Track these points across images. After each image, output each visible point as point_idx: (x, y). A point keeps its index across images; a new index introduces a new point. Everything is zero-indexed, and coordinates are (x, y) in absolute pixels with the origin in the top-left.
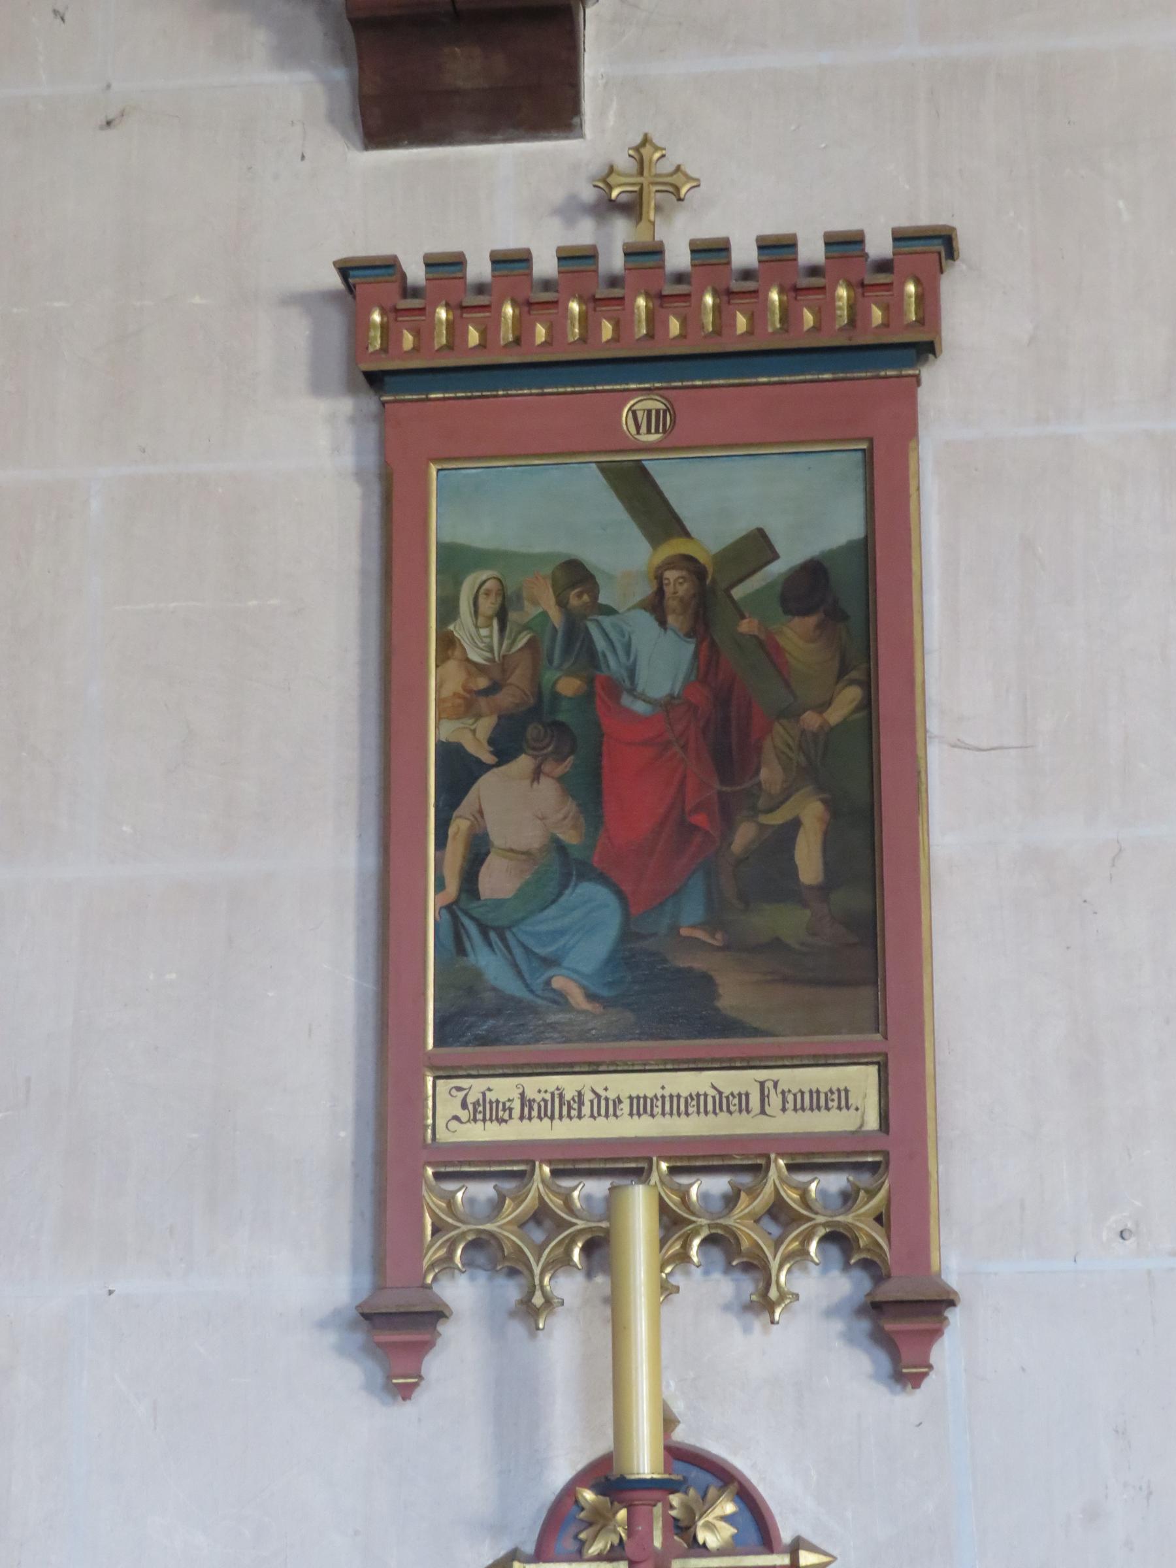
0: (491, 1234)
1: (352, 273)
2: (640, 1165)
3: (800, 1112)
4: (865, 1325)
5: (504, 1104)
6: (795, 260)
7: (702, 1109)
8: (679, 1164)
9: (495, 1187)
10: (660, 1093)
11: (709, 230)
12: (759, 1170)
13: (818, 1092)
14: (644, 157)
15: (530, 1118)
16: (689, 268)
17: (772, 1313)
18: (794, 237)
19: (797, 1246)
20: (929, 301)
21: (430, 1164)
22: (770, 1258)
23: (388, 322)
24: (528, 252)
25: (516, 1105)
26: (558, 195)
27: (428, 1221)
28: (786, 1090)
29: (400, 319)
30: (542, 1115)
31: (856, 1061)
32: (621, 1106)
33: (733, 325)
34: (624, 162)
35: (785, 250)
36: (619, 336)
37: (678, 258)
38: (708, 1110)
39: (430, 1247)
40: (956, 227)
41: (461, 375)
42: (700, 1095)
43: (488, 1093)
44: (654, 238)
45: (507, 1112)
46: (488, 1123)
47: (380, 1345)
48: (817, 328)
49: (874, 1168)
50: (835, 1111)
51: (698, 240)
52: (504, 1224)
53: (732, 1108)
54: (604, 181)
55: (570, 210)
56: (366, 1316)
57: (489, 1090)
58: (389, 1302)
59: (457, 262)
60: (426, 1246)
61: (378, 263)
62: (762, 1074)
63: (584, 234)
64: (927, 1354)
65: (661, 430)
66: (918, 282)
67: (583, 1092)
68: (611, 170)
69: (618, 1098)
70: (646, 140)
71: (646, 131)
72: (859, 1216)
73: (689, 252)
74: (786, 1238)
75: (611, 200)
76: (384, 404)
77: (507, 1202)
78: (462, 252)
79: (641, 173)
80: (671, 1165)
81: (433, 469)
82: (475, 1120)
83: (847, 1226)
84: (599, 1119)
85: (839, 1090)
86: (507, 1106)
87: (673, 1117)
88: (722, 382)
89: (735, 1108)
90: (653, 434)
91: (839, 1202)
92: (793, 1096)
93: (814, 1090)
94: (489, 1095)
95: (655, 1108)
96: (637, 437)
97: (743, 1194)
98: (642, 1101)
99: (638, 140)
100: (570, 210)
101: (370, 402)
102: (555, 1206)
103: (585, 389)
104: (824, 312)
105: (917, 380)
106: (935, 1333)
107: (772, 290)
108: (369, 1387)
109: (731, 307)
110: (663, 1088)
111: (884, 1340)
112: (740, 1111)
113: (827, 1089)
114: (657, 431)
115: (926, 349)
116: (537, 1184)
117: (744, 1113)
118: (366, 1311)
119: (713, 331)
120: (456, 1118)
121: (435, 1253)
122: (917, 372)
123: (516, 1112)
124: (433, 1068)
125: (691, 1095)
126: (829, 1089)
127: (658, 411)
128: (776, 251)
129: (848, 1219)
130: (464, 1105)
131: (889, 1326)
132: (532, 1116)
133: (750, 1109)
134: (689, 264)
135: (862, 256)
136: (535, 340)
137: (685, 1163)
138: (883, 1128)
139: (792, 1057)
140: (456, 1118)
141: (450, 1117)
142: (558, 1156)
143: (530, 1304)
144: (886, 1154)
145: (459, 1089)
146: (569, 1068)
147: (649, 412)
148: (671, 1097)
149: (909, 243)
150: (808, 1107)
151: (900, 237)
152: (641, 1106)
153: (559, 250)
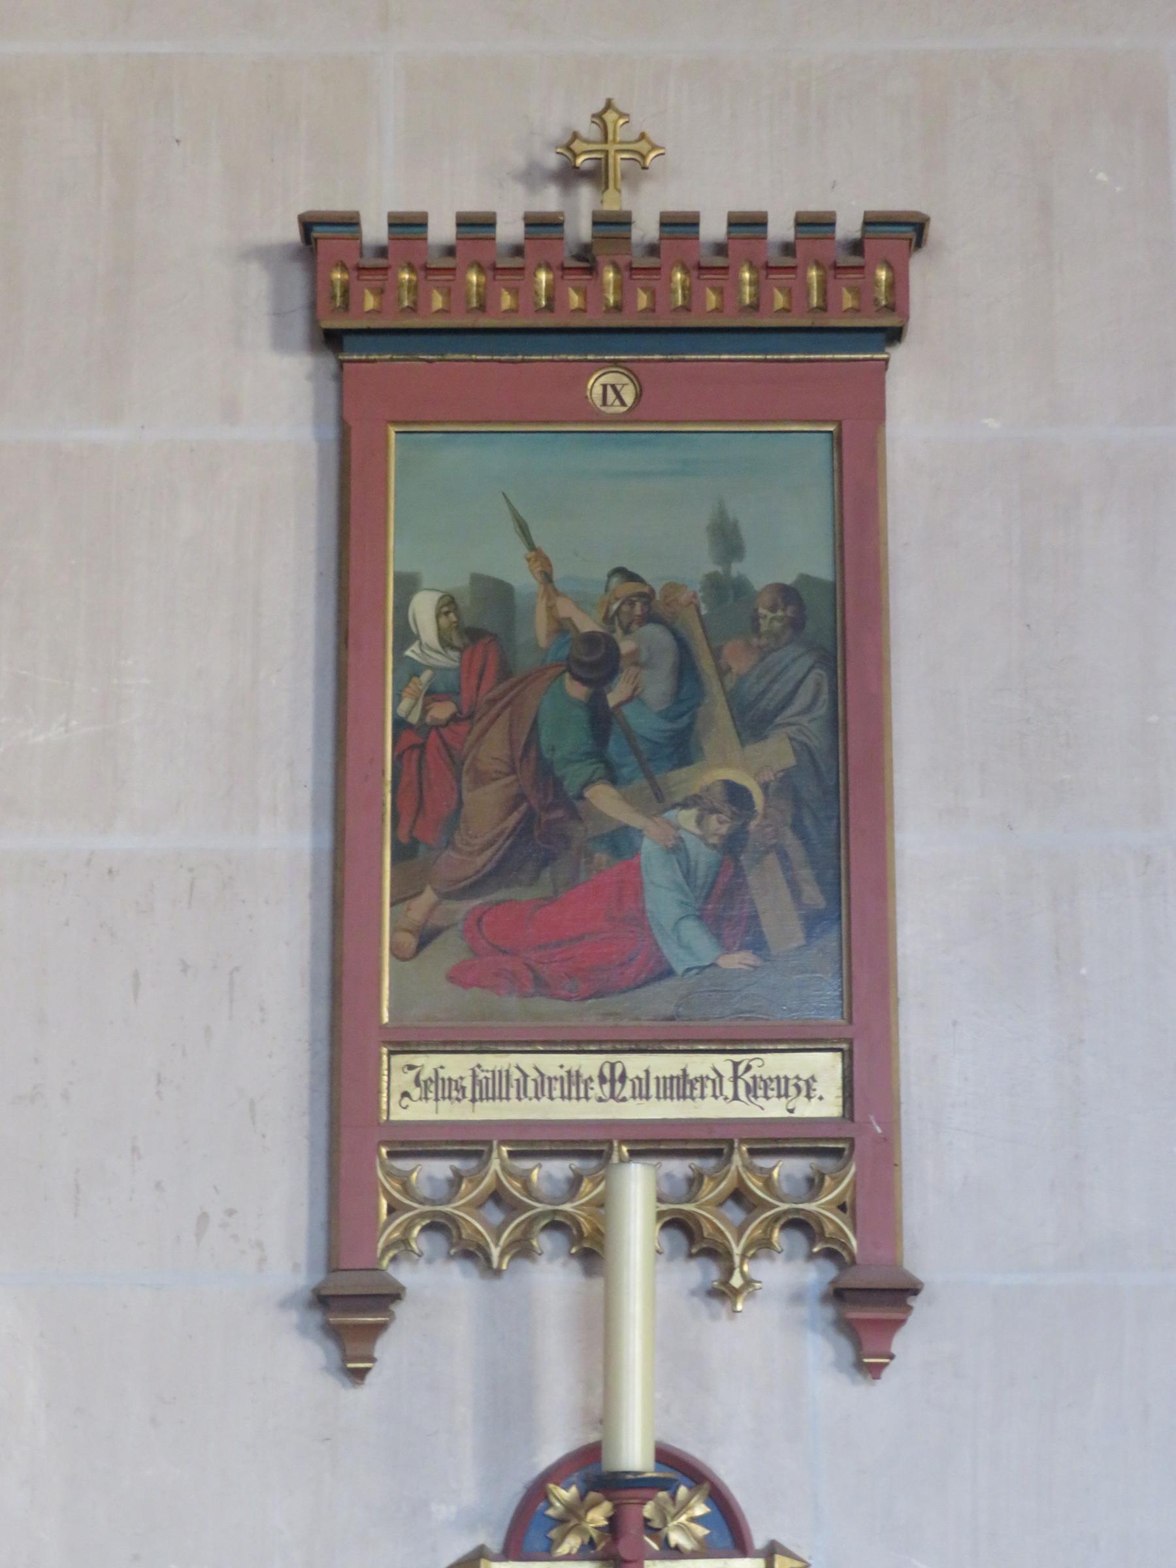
1: (316, 228)
2: (840, 1146)
4: (829, 1312)
5: (456, 1081)
8: (554, 1148)
11: (678, 202)
16: (726, 241)
17: (734, 1304)
18: (833, 214)
19: (760, 1233)
20: (899, 285)
21: (385, 1143)
22: (734, 1245)
23: (417, 281)
25: (467, 1084)
26: (519, 161)
27: (384, 1204)
29: (635, 277)
32: (592, 1085)
33: (498, 302)
34: (588, 129)
35: (552, 229)
36: (826, 305)
37: (646, 228)
39: (388, 1224)
40: (297, 215)
41: (719, 337)
43: (440, 1071)
48: (651, 309)
49: (837, 1153)
52: (582, 1204)
54: (568, 148)
55: (531, 176)
57: (442, 1067)
58: (348, 1284)
59: (350, 222)
60: (381, 1225)
61: (678, 221)
63: (549, 201)
64: (372, 1349)
66: (890, 267)
68: (575, 136)
70: (609, 105)
71: (609, 96)
72: (702, 1204)
73: (429, 225)
74: (749, 1225)
75: (575, 167)
77: (463, 1186)
79: (605, 140)
80: (630, 1148)
81: (392, 430)
82: (427, 1098)
83: (690, 1214)
88: (693, 357)
91: (803, 1187)
94: (442, 1073)
96: (603, 409)
97: (706, 1180)
99: (601, 105)
100: (531, 176)
101: (329, 362)
105: (887, 361)
106: (897, 1324)
108: (837, 1365)
109: (496, 283)
111: (848, 1328)
115: (895, 335)
116: (495, 1165)
118: (324, 1292)
119: (547, 306)
121: (392, 1233)
122: (885, 356)
124: (386, 1043)
128: (811, 229)
129: (812, 1207)
130: (417, 1082)
131: (854, 1314)
136: (637, 304)
137: (652, 1147)
138: (847, 1116)
139: (600, 1042)
140: (405, 1094)
142: (632, 1136)
144: (851, 1141)
145: (411, 1067)
146: (552, 1045)
150: (699, 1096)
153: (391, 216)
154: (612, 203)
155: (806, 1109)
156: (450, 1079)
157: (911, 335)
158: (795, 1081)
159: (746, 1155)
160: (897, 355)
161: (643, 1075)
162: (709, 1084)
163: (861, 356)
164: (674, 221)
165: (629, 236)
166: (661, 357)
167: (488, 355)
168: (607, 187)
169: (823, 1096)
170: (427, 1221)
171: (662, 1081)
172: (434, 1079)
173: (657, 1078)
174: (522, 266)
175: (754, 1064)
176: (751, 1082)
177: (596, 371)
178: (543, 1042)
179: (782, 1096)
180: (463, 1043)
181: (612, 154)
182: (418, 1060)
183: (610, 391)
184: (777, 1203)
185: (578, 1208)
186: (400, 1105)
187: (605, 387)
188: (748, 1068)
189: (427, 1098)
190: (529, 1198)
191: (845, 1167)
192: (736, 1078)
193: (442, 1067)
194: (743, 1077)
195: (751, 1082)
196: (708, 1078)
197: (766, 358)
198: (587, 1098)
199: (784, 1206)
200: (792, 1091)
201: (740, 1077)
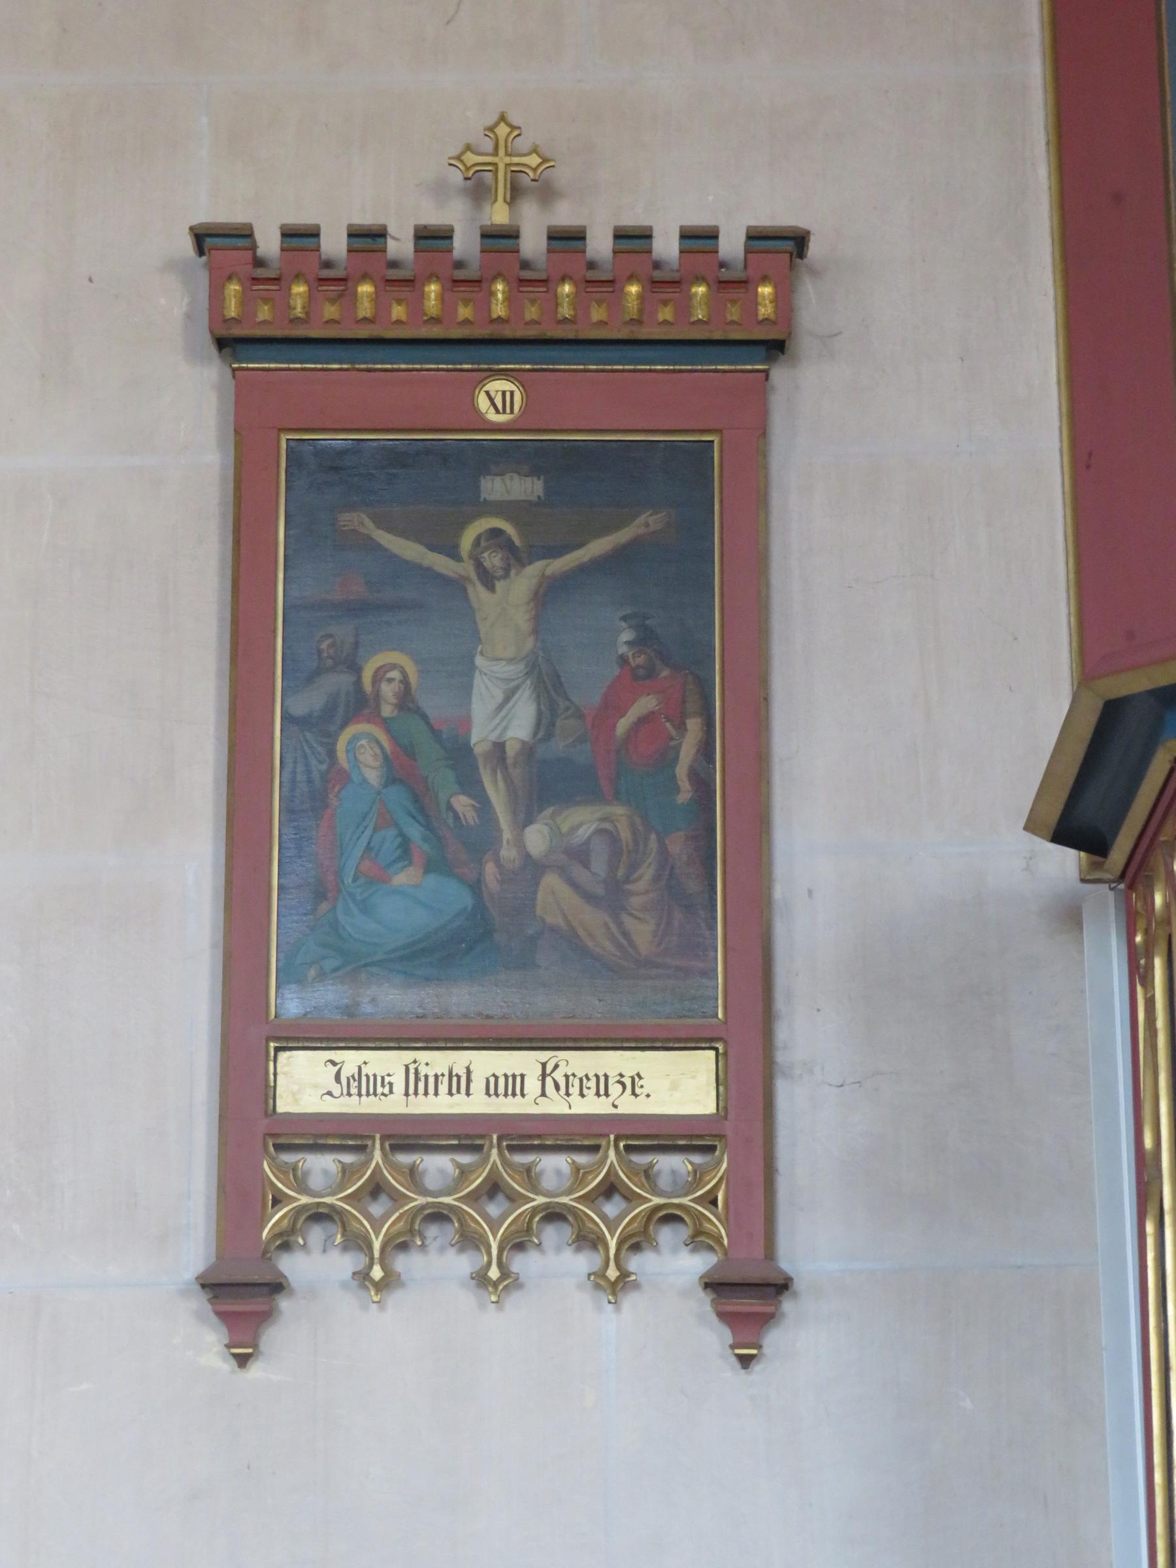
1: (209, 240)
6: (584, 252)
9: (453, 1160)
11: (565, 216)
14: (500, 138)
28: (439, 1074)
32: (641, 1083)
46: (364, 1098)
56: (708, 1286)
59: (711, 235)
62: (408, 1056)
67: (472, 1068)
69: (638, 1075)
70: (503, 118)
73: (322, 236)
76: (234, 370)
84: (457, 1097)
87: (418, 1096)
88: (726, 367)
89: (641, 1090)
92: (578, 1080)
95: (440, 1083)
99: (494, 118)
103: (292, 366)
104: (684, 306)
105: (766, 373)
113: (633, 1073)
117: (519, 1097)
120: (329, 1093)
123: (399, 1088)
126: (585, 1074)
130: (338, 1078)
132: (499, 1093)
133: (525, 1092)
135: (616, 252)
141: (325, 1092)
143: (486, 1277)
145: (334, 1063)
147: (504, 393)
153: (682, 228)
154: (499, 215)
157: (805, 342)
158: (618, 1078)
160: (779, 374)
163: (272, 366)
166: (470, 366)
167: (632, 365)
168: (496, 200)
169: (650, 1098)
173: (367, 1076)
174: (611, 279)
175: (562, 1064)
177: (475, 388)
178: (636, 1040)
179: (370, 1095)
180: (462, 1040)
181: (501, 167)
187: (512, 412)
188: (556, 1066)
189: (349, 1094)
193: (365, 1063)
194: (552, 1075)
197: (716, 369)
201: (549, 1075)
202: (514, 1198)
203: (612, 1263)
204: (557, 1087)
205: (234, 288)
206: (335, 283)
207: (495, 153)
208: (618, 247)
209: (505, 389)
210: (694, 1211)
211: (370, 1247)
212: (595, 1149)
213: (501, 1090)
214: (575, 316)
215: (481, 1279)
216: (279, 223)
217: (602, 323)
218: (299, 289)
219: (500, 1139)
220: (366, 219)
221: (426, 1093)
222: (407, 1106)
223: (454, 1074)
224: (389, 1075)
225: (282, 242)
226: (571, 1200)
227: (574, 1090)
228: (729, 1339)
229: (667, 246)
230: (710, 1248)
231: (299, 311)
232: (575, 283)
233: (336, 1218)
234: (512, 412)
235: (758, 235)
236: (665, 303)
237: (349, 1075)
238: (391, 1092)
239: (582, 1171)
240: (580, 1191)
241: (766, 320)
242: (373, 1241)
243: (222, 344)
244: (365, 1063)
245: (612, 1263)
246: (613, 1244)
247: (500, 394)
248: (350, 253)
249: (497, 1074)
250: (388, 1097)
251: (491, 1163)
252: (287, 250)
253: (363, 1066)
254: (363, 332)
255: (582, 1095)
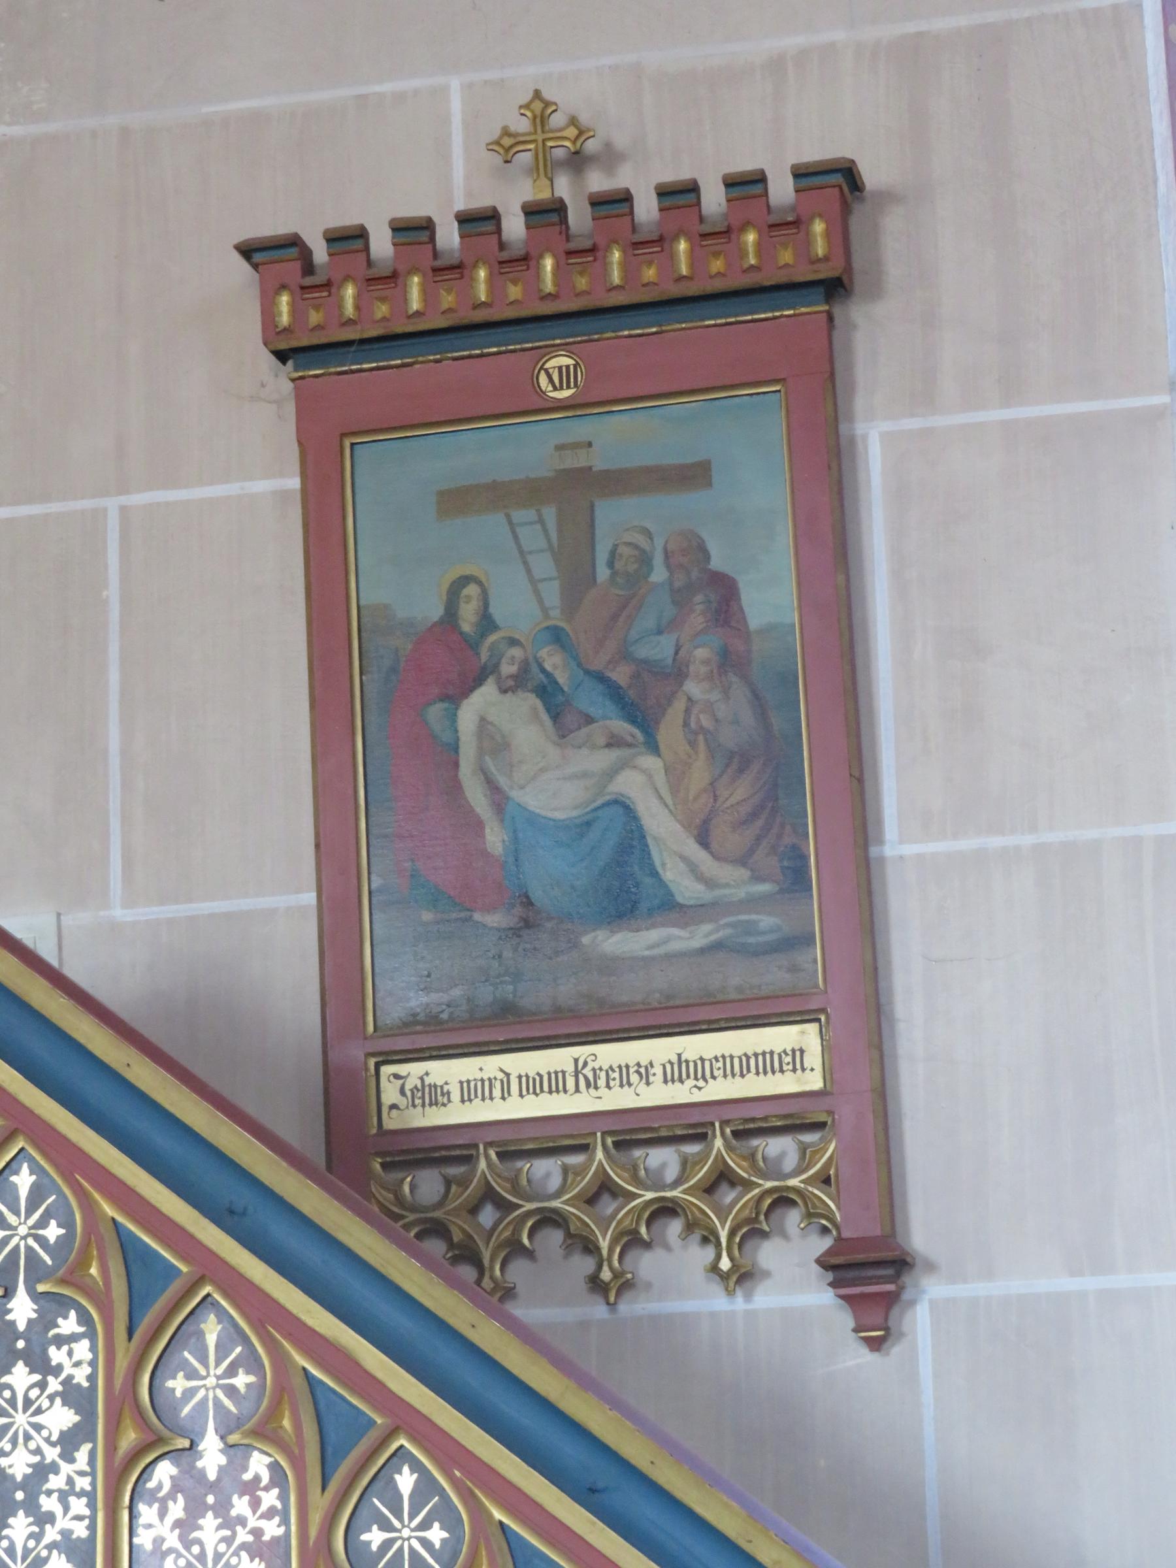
0: (555, 1211)
3: (467, 1103)
5: (442, 1087)
7: (798, 1066)
10: (479, 1076)
11: (598, 182)
12: (468, 1159)
13: (627, 1067)
15: (470, 1100)
20: (842, 237)
21: (378, 1154)
24: (495, 209)
30: (524, 1092)
31: (766, 1021)
38: (735, 1072)
42: (767, 1053)
44: (553, 194)
45: (446, 1096)
47: (842, 1297)
50: (789, 1074)
51: (404, 218)
53: (716, 1073)
61: (350, 233)
65: (572, 384)
70: (537, 94)
78: (296, 234)
82: (414, 1106)
85: (620, 1067)
86: (445, 1090)
90: (572, 388)
93: (623, 1065)
94: (428, 1081)
95: (494, 1089)
98: (768, 1056)
102: (385, 1199)
107: (282, 293)
110: (481, 1069)
112: (725, 1076)
114: (568, 387)
123: (456, 1096)
125: (611, 1068)
127: (568, 367)
134: (590, 217)
140: (394, 1107)
148: (549, 1074)
149: (617, 205)
151: (801, 173)
152: (533, 1085)
155: (786, 1084)
156: (435, 1086)
157: (859, 282)
159: (613, 1151)
161: (675, 1059)
162: (498, 1085)
164: (544, 208)
165: (662, 212)
170: (538, 1217)
171: (553, 1076)
172: (419, 1086)
176: (590, 1076)
182: (402, 1069)
183: (557, 384)
184: (520, 1202)
185: (687, 1192)
186: (690, 1089)
188: (585, 1064)
189: (414, 1106)
190: (515, 1196)
191: (825, 1142)
192: (577, 1073)
194: (583, 1072)
195: (590, 1076)
196: (495, 1079)
198: (803, 1069)
199: (650, 1195)
200: (634, 1078)
202: (748, 1185)
203: (724, 1254)
204: (588, 1085)
205: (284, 299)
206: (786, 227)
207: (535, 132)
208: (332, 251)
209: (569, 364)
210: (683, 1201)
211: (598, 1249)
212: (584, 1148)
213: (546, 1088)
214: (558, 292)
215: (595, 1284)
216: (322, 229)
217: (319, 327)
218: (349, 291)
219: (603, 1134)
220: (745, 164)
221: (758, 1073)
222: (424, 1116)
223: (683, 1059)
224: (446, 1083)
225: (659, 203)
226: (642, 1196)
227: (602, 1082)
228: (851, 1324)
229: (714, 199)
230: (825, 1230)
231: (684, 270)
232: (689, 239)
233: (679, 1210)
234: (576, 385)
235: (405, 226)
236: (716, 254)
237: (411, 1087)
238: (449, 1101)
239: (808, 1151)
240: (574, 1189)
241: (719, 274)
242: (481, 1252)
243: (282, 356)
244: (427, 1074)
245: (724, 1254)
246: (723, 1236)
247: (557, 370)
248: (798, 193)
249: (541, 1072)
250: (448, 1106)
251: (714, 1152)
252: (599, 219)
253: (425, 1077)
254: (316, 340)
255: (608, 1086)
